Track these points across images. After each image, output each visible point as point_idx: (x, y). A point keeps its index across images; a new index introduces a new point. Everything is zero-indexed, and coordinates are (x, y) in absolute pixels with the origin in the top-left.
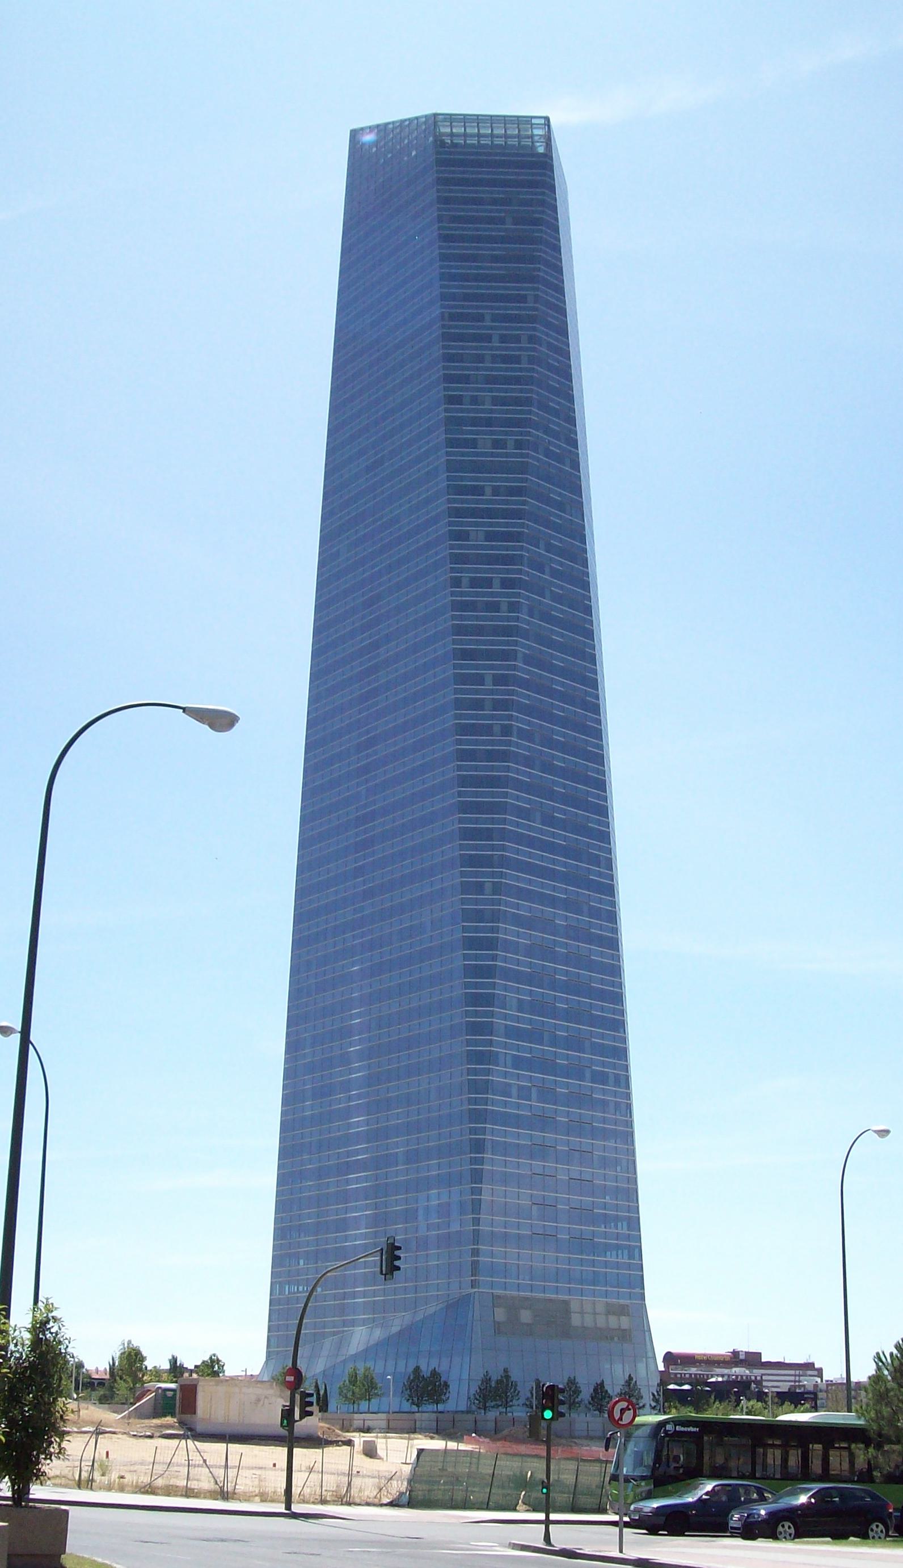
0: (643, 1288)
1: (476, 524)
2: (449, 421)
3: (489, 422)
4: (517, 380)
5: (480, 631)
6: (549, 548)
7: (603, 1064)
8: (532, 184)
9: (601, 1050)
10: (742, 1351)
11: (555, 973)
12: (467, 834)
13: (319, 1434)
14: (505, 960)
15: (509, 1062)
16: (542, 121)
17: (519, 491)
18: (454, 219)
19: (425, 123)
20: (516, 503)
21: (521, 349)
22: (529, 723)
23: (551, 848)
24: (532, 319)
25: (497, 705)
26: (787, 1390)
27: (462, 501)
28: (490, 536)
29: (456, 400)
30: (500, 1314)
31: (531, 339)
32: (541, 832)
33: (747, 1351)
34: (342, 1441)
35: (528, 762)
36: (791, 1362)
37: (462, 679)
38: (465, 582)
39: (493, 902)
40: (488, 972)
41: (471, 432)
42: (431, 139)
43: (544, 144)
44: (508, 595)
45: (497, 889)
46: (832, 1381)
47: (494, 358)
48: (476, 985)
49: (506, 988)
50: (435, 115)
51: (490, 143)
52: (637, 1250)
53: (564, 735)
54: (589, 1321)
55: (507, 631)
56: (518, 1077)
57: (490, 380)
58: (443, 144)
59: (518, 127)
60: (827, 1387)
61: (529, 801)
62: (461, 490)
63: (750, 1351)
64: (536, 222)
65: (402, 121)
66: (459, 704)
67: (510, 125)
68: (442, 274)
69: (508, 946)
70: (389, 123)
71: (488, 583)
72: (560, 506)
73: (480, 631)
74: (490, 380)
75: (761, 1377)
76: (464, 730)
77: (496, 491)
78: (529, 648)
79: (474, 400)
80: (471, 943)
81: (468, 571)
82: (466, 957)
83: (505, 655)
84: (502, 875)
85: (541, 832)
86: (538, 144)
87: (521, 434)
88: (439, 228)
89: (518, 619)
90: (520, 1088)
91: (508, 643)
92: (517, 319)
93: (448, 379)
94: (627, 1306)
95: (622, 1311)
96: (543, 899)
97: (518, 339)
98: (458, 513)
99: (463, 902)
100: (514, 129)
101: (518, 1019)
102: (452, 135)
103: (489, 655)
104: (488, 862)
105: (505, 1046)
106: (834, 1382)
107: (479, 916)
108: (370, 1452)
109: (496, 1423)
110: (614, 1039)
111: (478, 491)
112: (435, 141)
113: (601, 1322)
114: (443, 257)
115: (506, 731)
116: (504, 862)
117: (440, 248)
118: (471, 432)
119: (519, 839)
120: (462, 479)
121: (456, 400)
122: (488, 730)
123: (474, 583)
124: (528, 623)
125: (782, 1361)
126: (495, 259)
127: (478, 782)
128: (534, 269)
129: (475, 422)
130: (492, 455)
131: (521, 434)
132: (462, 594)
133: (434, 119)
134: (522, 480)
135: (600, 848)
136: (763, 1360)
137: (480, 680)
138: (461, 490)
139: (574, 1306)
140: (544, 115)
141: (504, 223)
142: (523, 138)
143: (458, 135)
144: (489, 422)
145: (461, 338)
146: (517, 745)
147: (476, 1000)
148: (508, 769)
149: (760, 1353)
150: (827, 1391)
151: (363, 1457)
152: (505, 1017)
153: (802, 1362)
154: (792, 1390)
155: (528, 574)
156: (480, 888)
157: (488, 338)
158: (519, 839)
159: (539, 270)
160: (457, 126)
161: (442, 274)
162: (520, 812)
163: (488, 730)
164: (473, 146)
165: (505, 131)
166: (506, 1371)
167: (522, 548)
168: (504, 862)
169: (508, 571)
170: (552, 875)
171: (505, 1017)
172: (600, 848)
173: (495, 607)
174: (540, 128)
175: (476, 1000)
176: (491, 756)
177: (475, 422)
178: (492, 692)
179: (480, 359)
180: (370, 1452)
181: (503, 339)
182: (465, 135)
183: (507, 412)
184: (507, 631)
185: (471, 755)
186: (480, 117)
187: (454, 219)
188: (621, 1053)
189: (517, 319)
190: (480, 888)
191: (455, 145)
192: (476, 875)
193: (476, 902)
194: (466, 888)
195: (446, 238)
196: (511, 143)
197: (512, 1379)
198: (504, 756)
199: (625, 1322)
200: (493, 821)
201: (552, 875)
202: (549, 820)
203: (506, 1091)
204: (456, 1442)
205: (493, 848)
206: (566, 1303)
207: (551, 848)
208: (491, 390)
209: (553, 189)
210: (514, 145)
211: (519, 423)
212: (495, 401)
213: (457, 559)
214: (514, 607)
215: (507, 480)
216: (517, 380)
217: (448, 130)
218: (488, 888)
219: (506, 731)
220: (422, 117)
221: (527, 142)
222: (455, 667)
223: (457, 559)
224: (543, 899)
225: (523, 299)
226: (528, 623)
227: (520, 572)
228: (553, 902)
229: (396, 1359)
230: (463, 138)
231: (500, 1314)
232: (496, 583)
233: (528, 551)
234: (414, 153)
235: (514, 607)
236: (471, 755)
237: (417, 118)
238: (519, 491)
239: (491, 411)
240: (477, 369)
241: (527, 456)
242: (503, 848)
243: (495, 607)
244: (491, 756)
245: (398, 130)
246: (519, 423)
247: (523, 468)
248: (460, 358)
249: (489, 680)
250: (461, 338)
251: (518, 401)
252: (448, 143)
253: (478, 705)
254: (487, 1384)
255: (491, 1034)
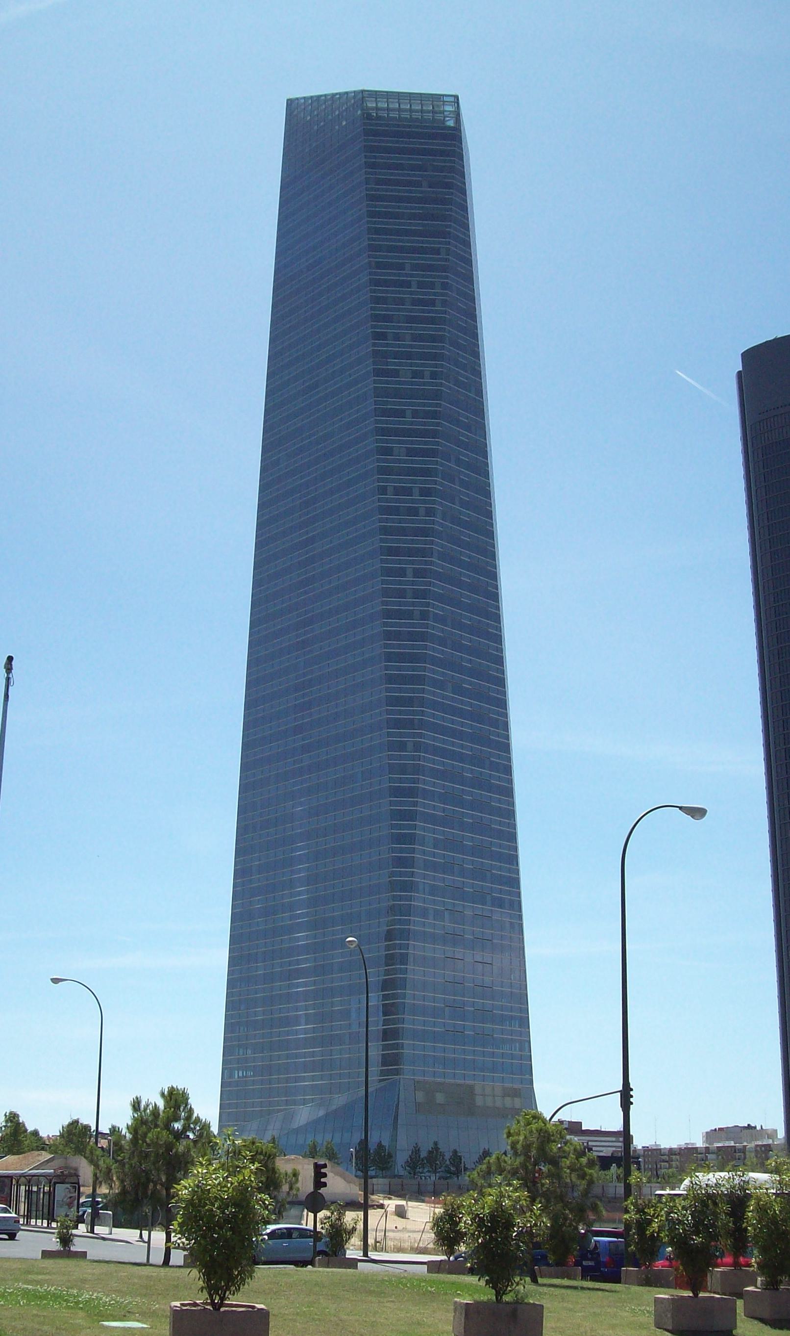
0: (531, 1075)
1: (399, 442)
2: (375, 353)
3: (409, 356)
4: (432, 321)
5: (403, 531)
6: (459, 462)
7: (501, 891)
8: (442, 153)
9: (500, 880)
10: (565, 1121)
11: (491, 823)
12: (392, 701)
13: (360, 1200)
14: (424, 806)
15: (421, 887)
16: (452, 99)
17: (435, 415)
18: (379, 182)
19: (354, 97)
20: (433, 424)
21: (435, 294)
22: (443, 609)
23: (461, 713)
24: (444, 269)
25: (416, 594)
26: (610, 1155)
27: (387, 422)
28: (410, 452)
29: (383, 336)
30: (420, 1096)
31: (445, 286)
32: (453, 699)
33: (570, 1120)
34: (376, 1205)
35: (442, 642)
36: (607, 1130)
37: (389, 572)
38: (390, 490)
39: (413, 758)
40: (410, 816)
41: (395, 364)
42: (359, 112)
43: (454, 119)
44: (425, 502)
45: (417, 747)
46: (648, 1147)
47: (415, 302)
48: (400, 827)
49: (424, 829)
50: (363, 91)
51: (409, 116)
52: (527, 1044)
53: (470, 619)
54: (489, 1102)
55: (424, 532)
56: (434, 902)
57: (411, 320)
58: (369, 117)
59: (410, 102)
60: (644, 1153)
61: (443, 674)
62: (385, 413)
63: (573, 1121)
64: (448, 186)
65: (334, 95)
66: (386, 593)
67: (414, 101)
68: (369, 228)
69: (426, 794)
70: (321, 96)
71: (408, 492)
72: (468, 428)
73: (403, 531)
74: (411, 320)
75: (588, 1143)
76: (388, 614)
77: (415, 414)
78: (442, 546)
79: (397, 337)
80: (396, 792)
81: (394, 481)
82: (391, 803)
83: (423, 552)
84: (420, 735)
85: (453, 699)
86: (448, 119)
87: (436, 366)
88: (367, 189)
89: (433, 522)
90: (435, 911)
91: (426, 542)
92: (431, 268)
93: (376, 318)
94: (520, 1089)
95: (516, 1093)
96: (453, 755)
97: (432, 285)
98: (383, 432)
99: (390, 757)
100: (406, 103)
101: (434, 855)
102: (377, 109)
103: (410, 552)
104: (410, 724)
105: (425, 877)
106: (650, 1148)
107: (403, 770)
108: (401, 1213)
109: (434, 1186)
110: (509, 870)
111: (401, 413)
112: (363, 114)
113: (499, 1104)
114: (372, 214)
115: (424, 616)
116: (422, 724)
117: (368, 206)
118: (395, 364)
119: (435, 705)
120: (387, 403)
121: (383, 336)
122: (410, 615)
123: (397, 491)
124: (441, 525)
125: (599, 1129)
126: (414, 216)
127: (401, 658)
128: (447, 226)
129: (396, 355)
130: (412, 384)
131: (436, 366)
132: (387, 500)
133: (363, 96)
134: (437, 405)
135: (498, 714)
136: (583, 1128)
137: (402, 572)
138: (385, 413)
139: (478, 1090)
140: (453, 93)
141: (421, 186)
142: (425, 113)
143: (382, 109)
144: (409, 356)
145: (386, 283)
146: (434, 628)
147: (399, 839)
148: (426, 647)
149: (581, 1123)
150: (644, 1156)
151: (396, 1218)
152: (424, 853)
153: (616, 1130)
154: (616, 1155)
155: (442, 485)
156: (402, 746)
157: (408, 284)
158: (435, 705)
159: (450, 227)
160: (393, 102)
161: (369, 228)
162: (435, 683)
163: (410, 615)
164: (394, 119)
165: (422, 107)
166: (436, 1143)
167: (437, 463)
168: (422, 724)
169: (426, 482)
170: (461, 735)
171: (424, 853)
172: (498, 714)
173: (413, 512)
174: (449, 105)
175: (399, 839)
176: (412, 637)
177: (396, 355)
178: (413, 583)
179: (402, 302)
180: (401, 1213)
181: (421, 285)
182: (388, 109)
183: (424, 347)
184: (424, 532)
185: (397, 636)
186: (378, 93)
187: (379, 182)
188: (515, 883)
189: (431, 268)
190: (402, 746)
191: (379, 118)
192: (401, 735)
193: (401, 758)
194: (391, 746)
195: (371, 198)
196: (415, 117)
197: (440, 1150)
198: (423, 637)
199: (518, 1103)
200: (413, 691)
201: (461, 735)
202: (458, 690)
203: (424, 913)
204: (405, 1200)
205: (414, 713)
206: (471, 1088)
207: (455, 712)
208: (411, 328)
209: (461, 157)
210: (407, 118)
211: (435, 357)
212: (415, 338)
213: (383, 471)
214: (430, 512)
215: (424, 405)
216: (432, 321)
217: (374, 105)
218: (410, 746)
219: (424, 616)
220: (351, 92)
221: (439, 117)
222: (382, 561)
223: (383, 471)
224: (453, 755)
225: (437, 252)
226: (441, 525)
227: (435, 483)
228: (461, 758)
229: (333, 1132)
230: (386, 112)
231: (420, 1096)
232: (416, 491)
233: (442, 465)
234: (344, 123)
235: (430, 512)
236: (397, 636)
237: (347, 93)
238: (435, 415)
239: (411, 346)
240: (399, 310)
241: (441, 385)
242: (422, 713)
243: (413, 512)
244: (412, 637)
245: (330, 102)
246: (435, 357)
247: (437, 395)
248: (384, 300)
249: (409, 572)
250: (386, 283)
251: (433, 339)
252: (373, 116)
253: (402, 594)
254: (416, 1153)
255: (413, 867)
